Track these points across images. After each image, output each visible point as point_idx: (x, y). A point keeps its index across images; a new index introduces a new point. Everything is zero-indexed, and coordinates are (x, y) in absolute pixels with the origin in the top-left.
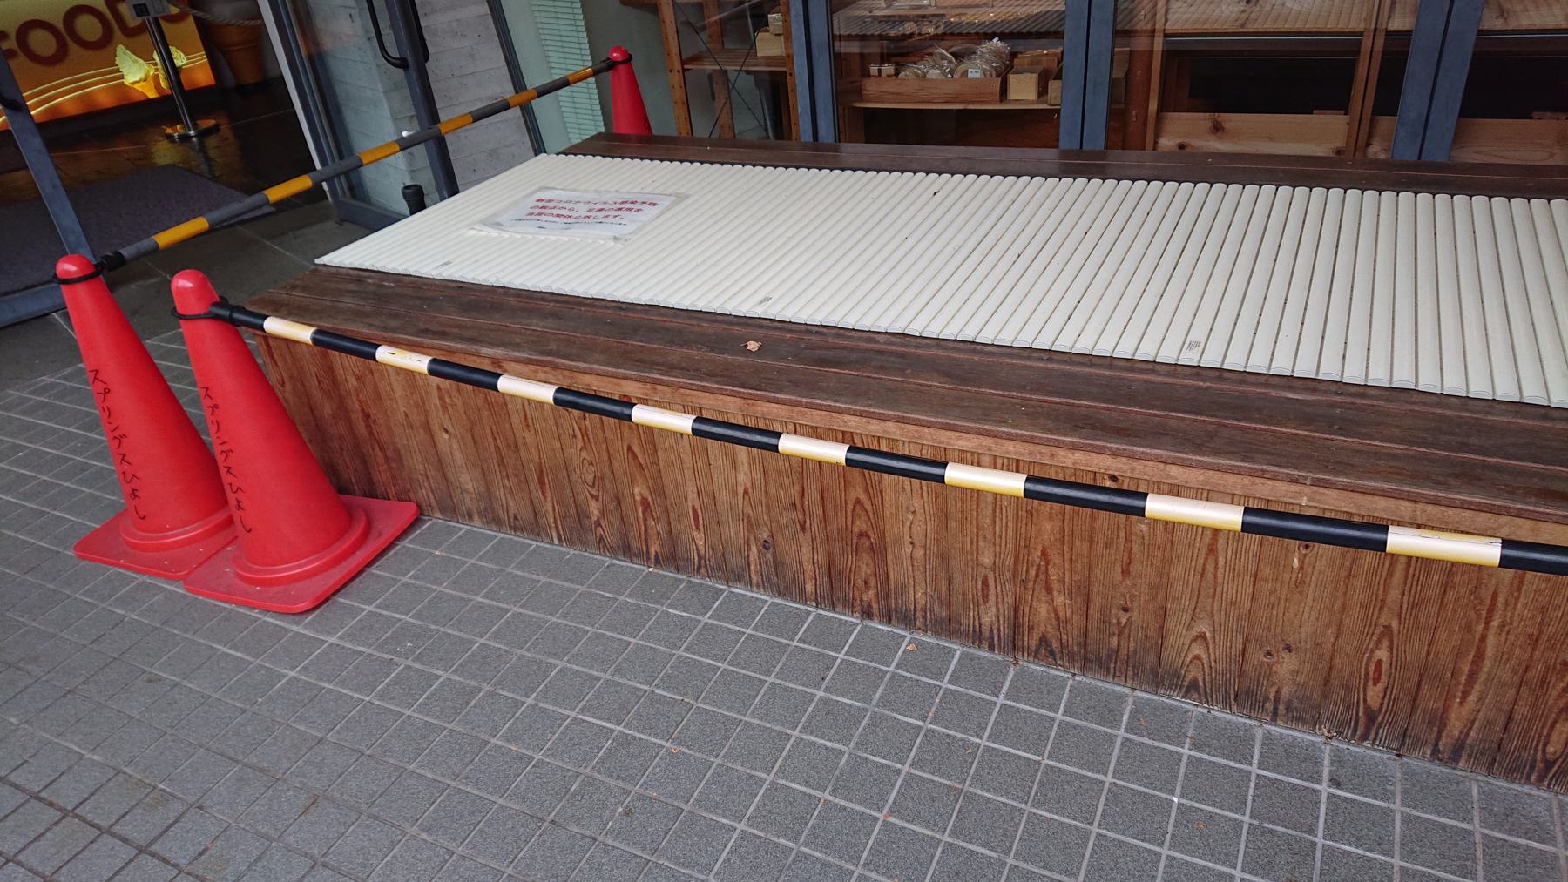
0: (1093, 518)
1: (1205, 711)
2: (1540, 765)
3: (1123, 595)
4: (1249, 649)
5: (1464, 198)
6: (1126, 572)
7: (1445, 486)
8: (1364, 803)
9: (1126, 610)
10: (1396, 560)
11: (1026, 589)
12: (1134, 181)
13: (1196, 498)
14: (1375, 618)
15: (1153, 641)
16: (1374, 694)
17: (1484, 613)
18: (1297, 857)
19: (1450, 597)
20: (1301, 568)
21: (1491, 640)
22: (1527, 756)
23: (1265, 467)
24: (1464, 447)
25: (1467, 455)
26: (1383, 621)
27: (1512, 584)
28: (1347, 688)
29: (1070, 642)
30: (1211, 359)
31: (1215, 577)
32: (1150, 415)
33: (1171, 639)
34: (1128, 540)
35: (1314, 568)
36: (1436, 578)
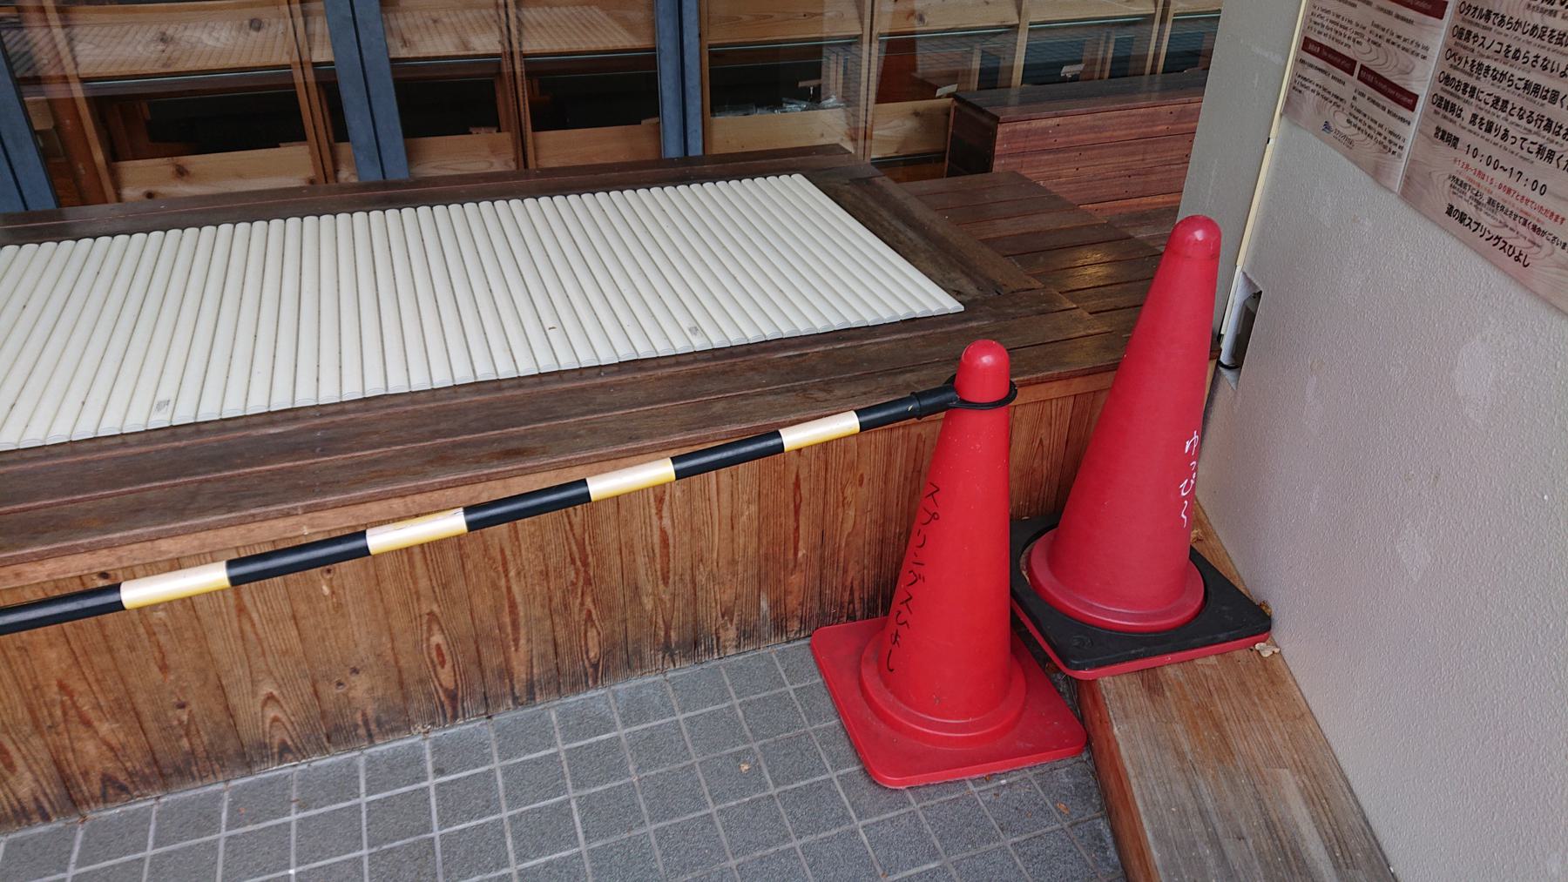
0: (101, 626)
1: (305, 766)
2: (590, 670)
3: (172, 693)
4: (321, 688)
5: (298, 220)
6: (164, 668)
7: (425, 475)
8: (468, 777)
9: (182, 706)
10: (412, 553)
11: (58, 734)
12: (148, 233)
13: (201, 564)
14: (416, 610)
15: (224, 724)
16: (446, 676)
17: (500, 569)
18: (418, 862)
19: (469, 566)
20: (333, 593)
21: (515, 589)
22: (579, 668)
23: (253, 511)
24: (436, 434)
25: (439, 441)
26: (425, 609)
27: (510, 537)
28: (421, 681)
29: (138, 767)
30: (184, 416)
31: (256, 634)
32: (124, 493)
33: (241, 716)
34: (151, 634)
35: (344, 588)
36: (451, 555)
